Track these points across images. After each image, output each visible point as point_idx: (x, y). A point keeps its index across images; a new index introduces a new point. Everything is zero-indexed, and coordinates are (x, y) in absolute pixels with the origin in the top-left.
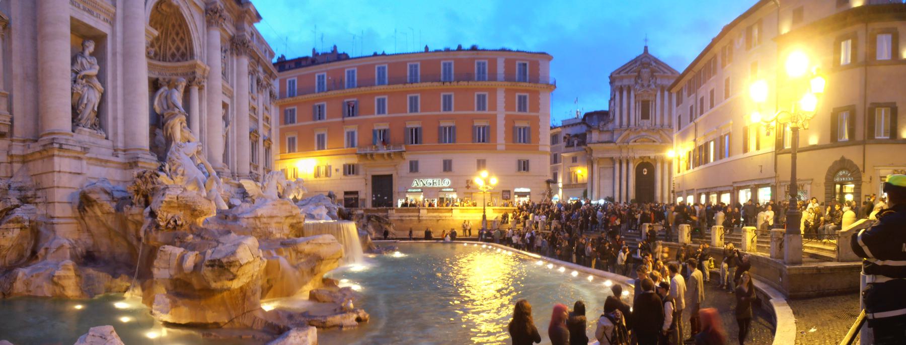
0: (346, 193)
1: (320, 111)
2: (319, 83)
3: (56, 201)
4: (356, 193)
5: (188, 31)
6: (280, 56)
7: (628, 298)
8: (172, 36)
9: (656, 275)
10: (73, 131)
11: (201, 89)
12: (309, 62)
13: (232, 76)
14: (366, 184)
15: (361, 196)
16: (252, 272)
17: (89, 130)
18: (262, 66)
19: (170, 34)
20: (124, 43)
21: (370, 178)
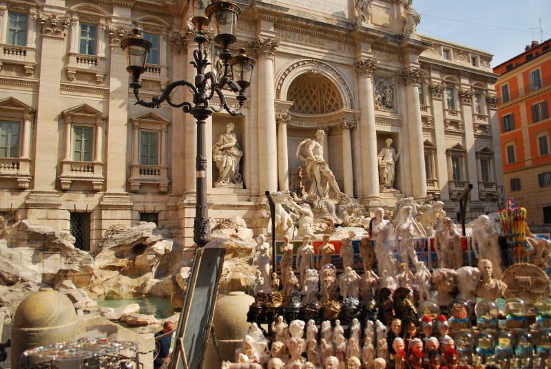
6: (530, 44)
19: (324, 92)
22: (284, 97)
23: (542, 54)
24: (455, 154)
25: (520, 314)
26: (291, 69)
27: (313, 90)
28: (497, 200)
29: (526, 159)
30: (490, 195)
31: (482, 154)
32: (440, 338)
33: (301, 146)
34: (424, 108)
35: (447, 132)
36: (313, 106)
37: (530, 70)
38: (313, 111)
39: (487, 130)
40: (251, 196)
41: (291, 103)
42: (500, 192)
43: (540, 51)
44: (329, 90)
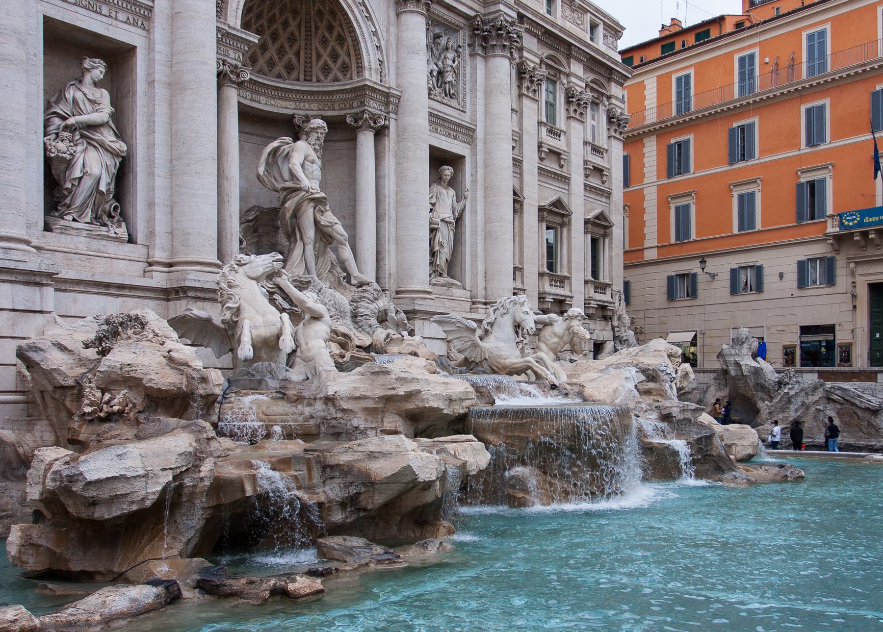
0: (805, 330)
1: (743, 139)
2: (679, 94)
4: (830, 329)
6: (668, 23)
7: (645, 479)
9: (677, 448)
10: (47, 228)
11: (380, 133)
12: (729, 27)
14: (855, 307)
15: (841, 337)
16: (143, 493)
17: (87, 226)
18: (579, 60)
19: (317, 28)
20: (171, 64)
21: (863, 293)
23: (693, 47)
24: (596, 230)
28: (611, 318)
29: (647, 244)
30: (603, 308)
31: (550, 212)
32: (280, 247)
34: (593, 119)
35: (588, 188)
36: (285, 59)
37: (672, 72)
38: (284, 73)
39: (604, 179)
40: (150, 264)
41: (254, 39)
42: (617, 304)
43: (691, 40)
44: (330, 28)
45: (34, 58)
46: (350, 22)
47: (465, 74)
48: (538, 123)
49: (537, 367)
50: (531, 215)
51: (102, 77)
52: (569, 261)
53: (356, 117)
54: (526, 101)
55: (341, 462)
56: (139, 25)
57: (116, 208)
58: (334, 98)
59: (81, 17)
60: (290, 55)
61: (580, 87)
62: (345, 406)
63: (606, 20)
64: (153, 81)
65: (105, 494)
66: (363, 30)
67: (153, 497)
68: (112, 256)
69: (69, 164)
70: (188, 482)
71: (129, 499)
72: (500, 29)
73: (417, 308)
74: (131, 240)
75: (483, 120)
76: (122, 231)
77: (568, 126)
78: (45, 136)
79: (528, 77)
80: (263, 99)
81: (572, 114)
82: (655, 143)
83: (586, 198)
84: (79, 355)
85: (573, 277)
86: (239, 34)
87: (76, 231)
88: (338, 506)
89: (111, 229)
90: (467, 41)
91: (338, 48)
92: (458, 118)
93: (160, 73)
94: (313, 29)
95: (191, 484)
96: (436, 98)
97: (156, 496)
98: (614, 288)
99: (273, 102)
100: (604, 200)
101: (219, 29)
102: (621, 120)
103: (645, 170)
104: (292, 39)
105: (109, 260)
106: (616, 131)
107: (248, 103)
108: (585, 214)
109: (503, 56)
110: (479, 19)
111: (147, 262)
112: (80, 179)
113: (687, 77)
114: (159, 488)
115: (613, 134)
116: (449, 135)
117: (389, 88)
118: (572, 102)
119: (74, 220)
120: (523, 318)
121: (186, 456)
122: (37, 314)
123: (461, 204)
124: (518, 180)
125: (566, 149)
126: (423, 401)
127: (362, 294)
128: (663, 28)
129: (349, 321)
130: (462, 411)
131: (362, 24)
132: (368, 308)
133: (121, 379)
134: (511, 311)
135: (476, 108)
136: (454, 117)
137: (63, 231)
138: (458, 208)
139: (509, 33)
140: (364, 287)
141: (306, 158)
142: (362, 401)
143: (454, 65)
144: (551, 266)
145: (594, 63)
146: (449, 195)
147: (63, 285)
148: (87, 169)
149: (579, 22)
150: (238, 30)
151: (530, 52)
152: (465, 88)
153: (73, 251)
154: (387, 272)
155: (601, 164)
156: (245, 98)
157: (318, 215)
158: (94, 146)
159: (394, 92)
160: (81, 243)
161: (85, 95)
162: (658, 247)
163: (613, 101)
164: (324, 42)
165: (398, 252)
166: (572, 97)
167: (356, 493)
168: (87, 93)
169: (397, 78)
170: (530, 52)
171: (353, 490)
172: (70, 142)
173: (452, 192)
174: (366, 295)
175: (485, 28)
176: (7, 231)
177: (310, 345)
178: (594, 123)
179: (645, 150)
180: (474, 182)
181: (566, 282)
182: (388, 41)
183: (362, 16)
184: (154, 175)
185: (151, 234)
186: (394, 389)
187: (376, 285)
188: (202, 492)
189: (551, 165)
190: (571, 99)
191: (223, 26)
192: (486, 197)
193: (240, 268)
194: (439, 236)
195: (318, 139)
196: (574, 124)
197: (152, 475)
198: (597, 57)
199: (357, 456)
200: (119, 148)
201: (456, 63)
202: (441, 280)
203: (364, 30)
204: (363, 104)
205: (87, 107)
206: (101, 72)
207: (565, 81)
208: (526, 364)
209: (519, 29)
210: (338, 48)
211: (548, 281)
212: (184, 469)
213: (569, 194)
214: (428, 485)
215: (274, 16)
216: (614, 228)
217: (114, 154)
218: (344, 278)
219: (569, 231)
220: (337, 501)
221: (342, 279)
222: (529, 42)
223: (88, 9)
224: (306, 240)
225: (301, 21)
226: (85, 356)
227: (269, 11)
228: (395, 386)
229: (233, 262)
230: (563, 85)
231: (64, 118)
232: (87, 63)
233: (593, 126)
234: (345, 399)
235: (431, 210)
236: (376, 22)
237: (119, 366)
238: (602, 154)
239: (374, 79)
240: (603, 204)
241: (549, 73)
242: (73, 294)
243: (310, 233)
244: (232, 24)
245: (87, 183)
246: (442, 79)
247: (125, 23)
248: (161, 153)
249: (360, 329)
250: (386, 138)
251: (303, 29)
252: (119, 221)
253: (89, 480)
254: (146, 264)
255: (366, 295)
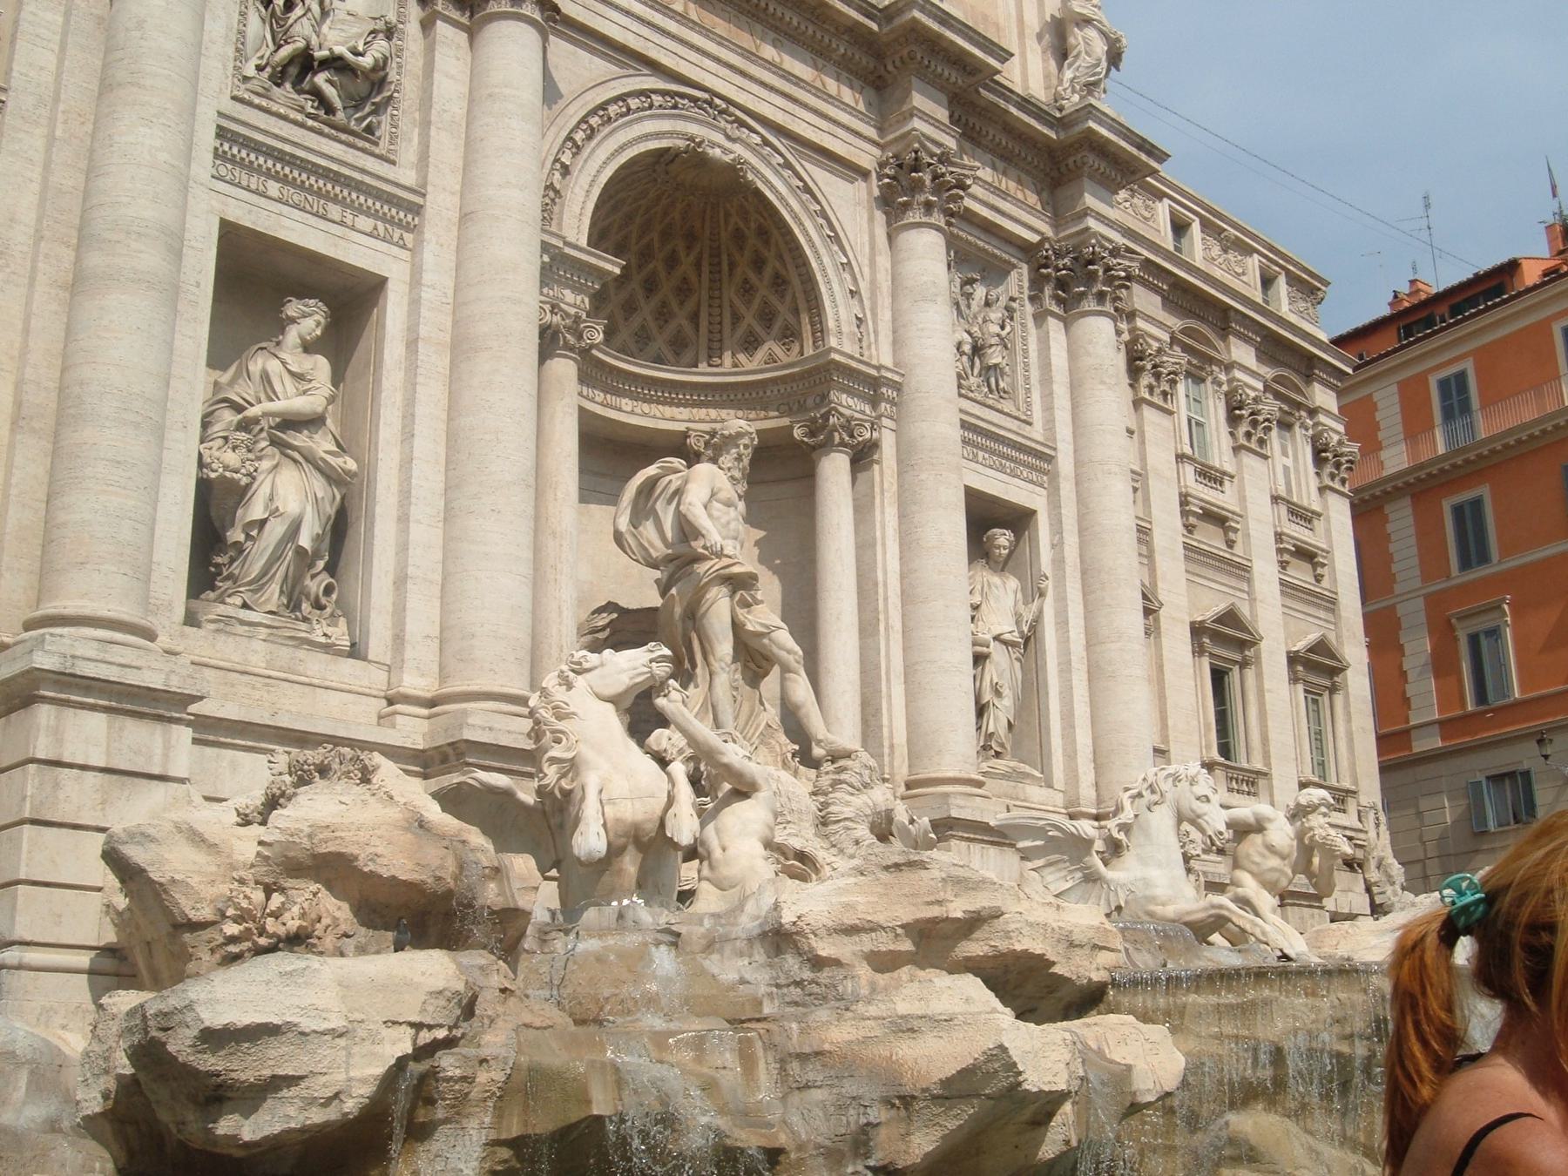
3: (86, 976)
5: (796, 248)
6: (1405, 289)
8: (739, 271)
10: (191, 620)
11: (863, 457)
13: (1048, 396)
19: (732, 266)
22: (576, 225)
25: (487, 1120)
26: (579, 136)
27: (682, 254)
31: (1217, 637)
33: (640, 492)
34: (1285, 454)
36: (672, 327)
38: (668, 353)
39: (1319, 571)
41: (613, 267)
42: (1372, 834)
44: (758, 264)
45: (193, 289)
46: (798, 247)
47: (1025, 351)
48: (1177, 456)
49: (1241, 916)
50: (1177, 643)
51: (318, 332)
52: (1265, 741)
53: (813, 427)
54: (1147, 412)
55: (827, 1047)
56: (395, 240)
57: (328, 590)
58: (769, 393)
59: (288, 223)
60: (681, 320)
61: (1254, 389)
62: (825, 949)
63: (1291, 268)
64: (416, 340)
65: (245, 1067)
66: (823, 262)
67: (361, 1092)
68: (316, 681)
69: (239, 493)
70: (448, 1063)
71: (304, 1093)
72: (1091, 262)
73: (954, 814)
74: (356, 651)
75: (1070, 438)
76: (340, 634)
77: (1239, 466)
78: (202, 442)
79: (1149, 366)
80: (627, 404)
81: (1243, 441)
82: (1409, 511)
83: (1286, 610)
84: (229, 856)
85: (1275, 772)
86: (584, 257)
87: (246, 628)
88: (821, 1160)
89: (317, 627)
90: (1026, 292)
91: (774, 300)
92: (1018, 434)
93: (435, 324)
94: (725, 267)
95: (458, 1072)
96: (971, 395)
97: (367, 1090)
98: (1364, 800)
99: (646, 408)
100: (1322, 614)
101: (545, 247)
102: (1342, 455)
103: (1395, 568)
104: (684, 290)
105: (307, 689)
106: (1332, 476)
107: (599, 410)
108: (1287, 644)
109: (1100, 313)
110: (1047, 246)
111: (385, 698)
112: (262, 523)
113: (1461, 377)
114: (379, 1070)
115: (1328, 481)
116: (1002, 470)
117: (878, 368)
118: (1241, 417)
119: (245, 606)
120: (1199, 812)
121: (449, 1000)
122: (156, 782)
123: (1034, 606)
124: (1146, 569)
125: (1237, 510)
126: (1007, 935)
127: (837, 777)
128: (1396, 297)
129: (810, 832)
130: (1097, 976)
131: (822, 251)
132: (848, 804)
133: (309, 862)
134: (1169, 796)
135: (1053, 414)
136: (1010, 430)
137: (222, 625)
138: (1028, 616)
139: (1108, 269)
140: (842, 763)
141: (713, 495)
142: (865, 937)
143: (1004, 333)
144: (1225, 750)
145: (1274, 347)
146: (1004, 594)
147: (212, 731)
148: (279, 503)
149: (1240, 271)
150: (580, 249)
151: (1149, 319)
152: (1027, 378)
153: (239, 667)
154: (886, 743)
155: (1309, 541)
156: (592, 400)
157: (741, 613)
158: (295, 461)
159: (889, 375)
160: (256, 652)
161: (284, 363)
162: (1441, 723)
163: (1322, 418)
164: (747, 290)
165: (911, 697)
166: (1240, 408)
167: (868, 1124)
168: (289, 361)
169: (894, 352)
170: (1149, 319)
171: (854, 1118)
172: (249, 451)
173: (1013, 583)
174: (843, 776)
175: (1061, 263)
176: (110, 607)
177: (731, 852)
178: (1289, 462)
179: (1390, 528)
180: (1059, 562)
181: (1262, 782)
182: (873, 282)
183: (821, 236)
184: (408, 520)
185: (399, 640)
186: (939, 903)
187: (864, 756)
188: (485, 1100)
189: (1210, 539)
190: (1237, 412)
191: (554, 241)
192: (1086, 591)
193: (580, 677)
194: (991, 672)
195: (739, 458)
196: (1249, 460)
197: (364, 1034)
198: (1281, 331)
199: (872, 1029)
200: (342, 465)
201: (1008, 329)
202: (1002, 765)
203: (826, 260)
204: (824, 397)
205: (288, 386)
206: (318, 324)
207: (1223, 377)
208: (1213, 912)
209: (1128, 263)
210: (774, 300)
211: (1224, 780)
212: (441, 1034)
213: (1252, 601)
214: (1049, 1103)
215: (649, 246)
216: (1349, 672)
217: (332, 477)
218: (794, 755)
219: (1259, 676)
220: (818, 1146)
221: (789, 756)
222: (1144, 300)
223: (303, 210)
224: (716, 665)
225: (701, 253)
226: (241, 858)
227: (640, 237)
228: (941, 896)
229: (565, 668)
230: (1220, 384)
231: (238, 409)
232: (293, 308)
233: (1286, 468)
234: (822, 932)
235: (973, 618)
236: (847, 248)
237: (307, 830)
238: (1310, 522)
239: (847, 349)
240: (1321, 623)
241: (1189, 362)
242: (229, 753)
243: (724, 647)
244: (571, 239)
245: (275, 530)
246: (981, 362)
247: (369, 235)
248: (428, 479)
249: (834, 851)
250: (876, 467)
251: (706, 268)
252: (332, 615)
253: (207, 1024)
254: (384, 702)
255: (843, 776)
